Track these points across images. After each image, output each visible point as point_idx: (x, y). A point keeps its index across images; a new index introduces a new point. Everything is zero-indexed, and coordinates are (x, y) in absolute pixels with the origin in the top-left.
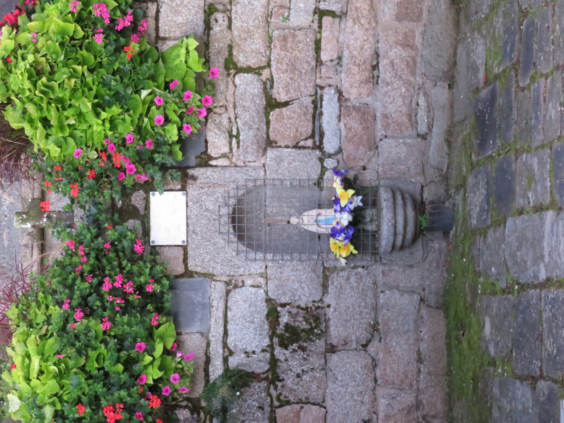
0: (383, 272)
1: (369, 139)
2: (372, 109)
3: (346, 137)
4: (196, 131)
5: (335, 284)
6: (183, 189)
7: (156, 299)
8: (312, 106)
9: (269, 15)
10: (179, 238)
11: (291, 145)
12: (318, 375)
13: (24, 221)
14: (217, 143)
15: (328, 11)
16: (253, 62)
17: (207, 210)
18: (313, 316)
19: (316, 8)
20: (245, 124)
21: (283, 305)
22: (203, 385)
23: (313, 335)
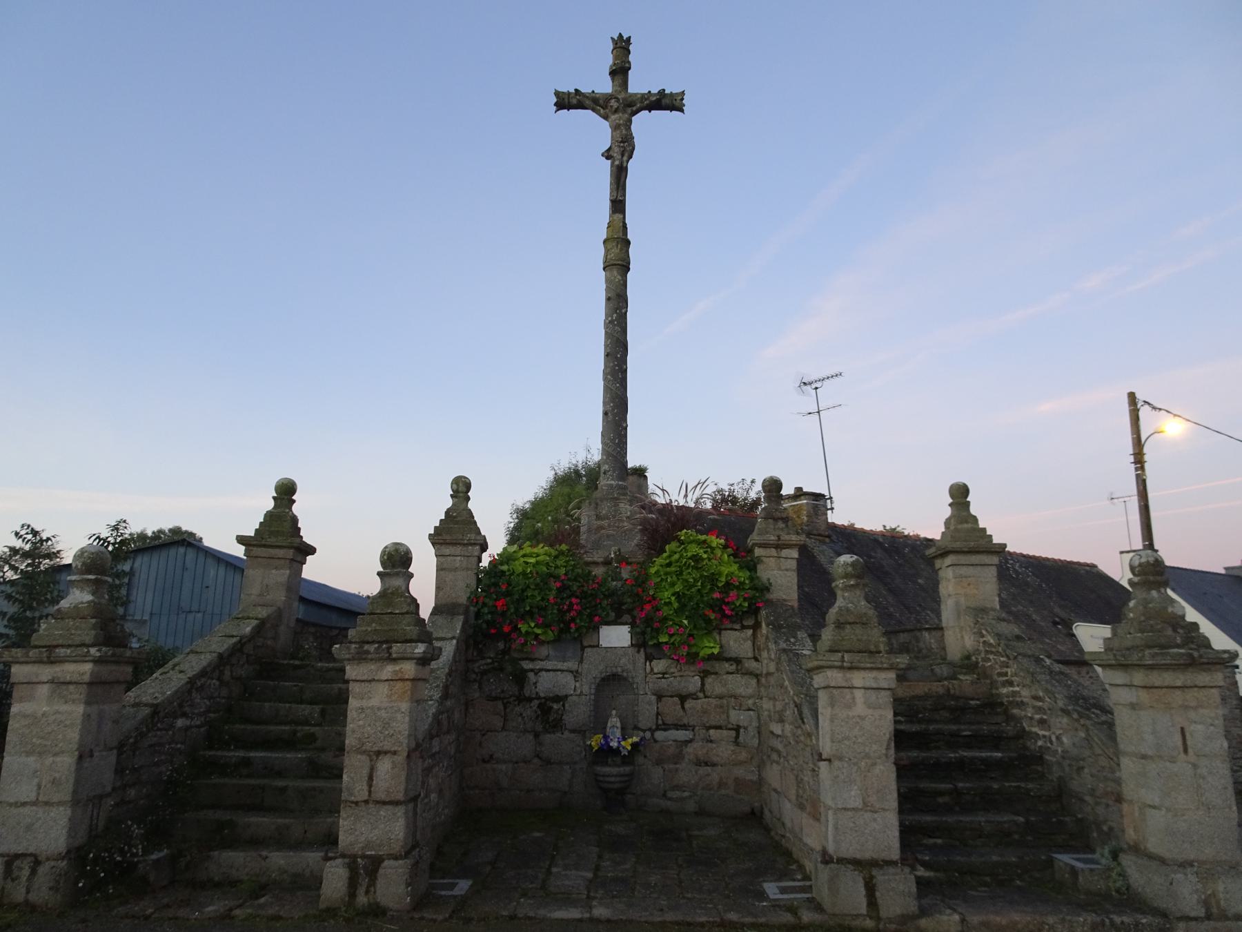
7: (565, 630)
9: (736, 697)
10: (604, 643)
14: (659, 665)
16: (707, 687)
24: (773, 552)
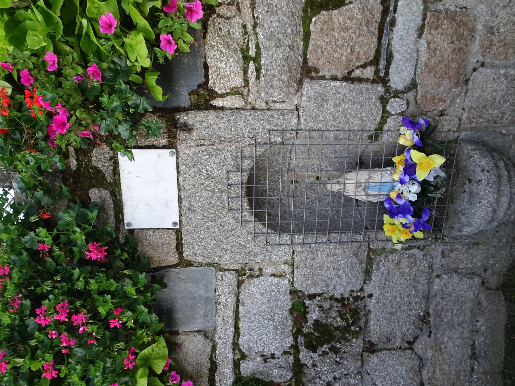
0: (443, 253)
3: (426, 65)
4: (186, 49)
6: (170, 146)
8: (381, 8)
10: (169, 218)
12: (352, 381)
14: (224, 70)
17: (209, 177)
20: (270, 37)
21: (312, 297)
23: (349, 333)
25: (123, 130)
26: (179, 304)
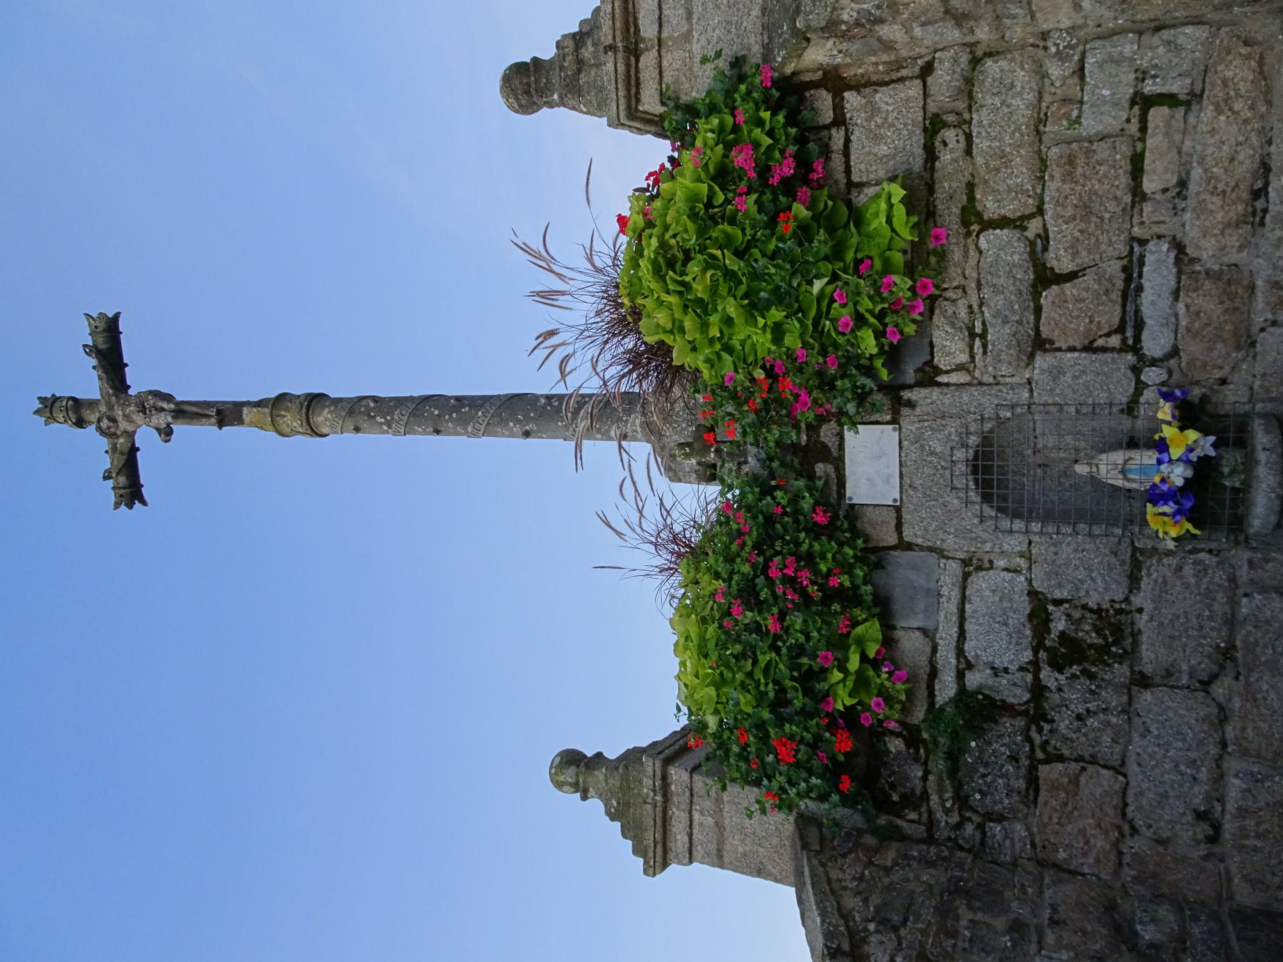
0: (1250, 562)
1: (1235, 332)
2: (1246, 274)
3: (1188, 330)
5: (1155, 576)
6: (894, 421)
8: (1123, 276)
9: (1040, 121)
10: (890, 495)
11: (1079, 346)
12: (1114, 720)
13: (687, 456)
14: (949, 347)
15: (1161, 95)
16: (1010, 209)
17: (932, 453)
18: (1110, 625)
19: (1136, 93)
20: (997, 314)
21: (1058, 602)
22: (925, 707)
24: (648, 60)
25: (851, 408)
26: (897, 593)
